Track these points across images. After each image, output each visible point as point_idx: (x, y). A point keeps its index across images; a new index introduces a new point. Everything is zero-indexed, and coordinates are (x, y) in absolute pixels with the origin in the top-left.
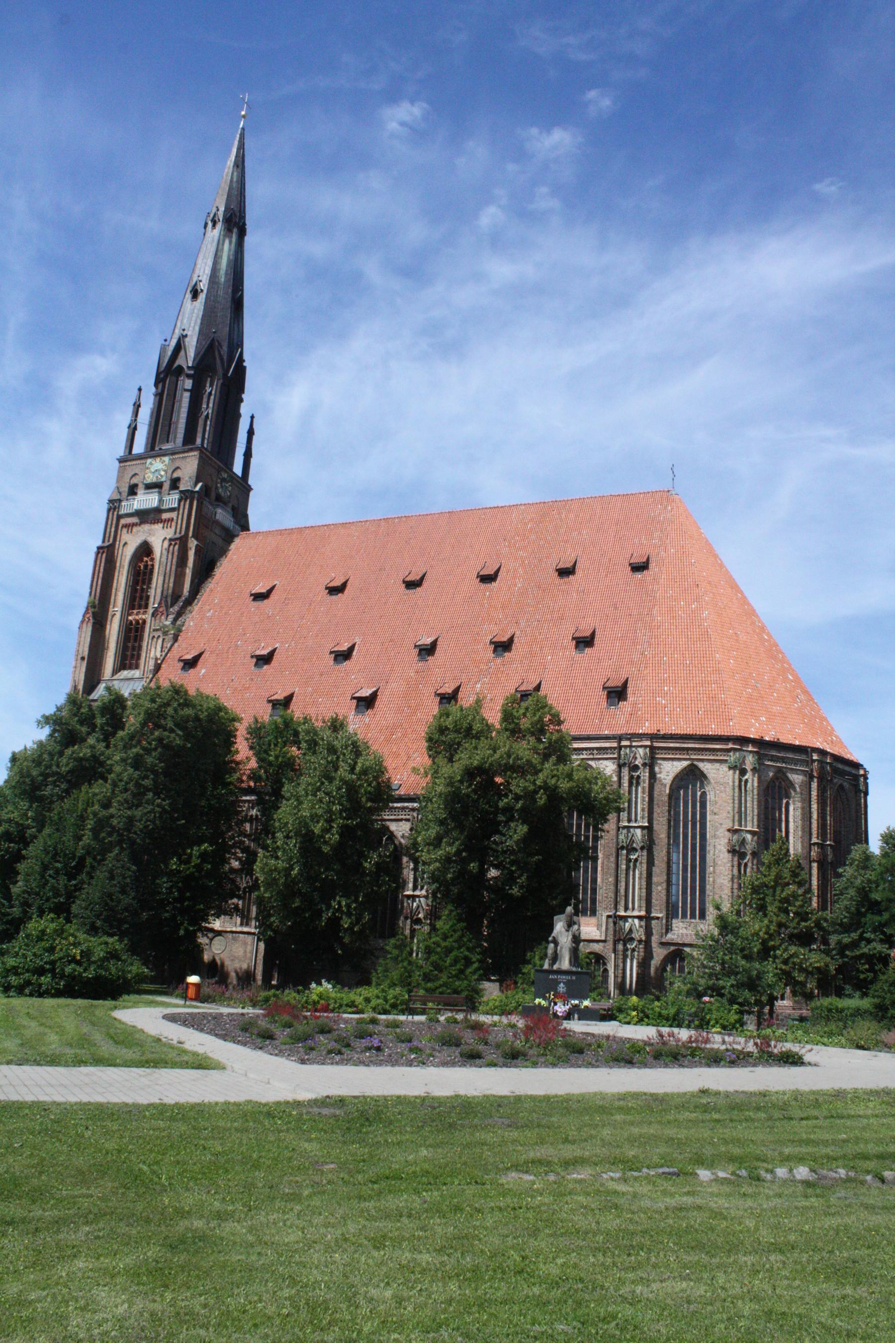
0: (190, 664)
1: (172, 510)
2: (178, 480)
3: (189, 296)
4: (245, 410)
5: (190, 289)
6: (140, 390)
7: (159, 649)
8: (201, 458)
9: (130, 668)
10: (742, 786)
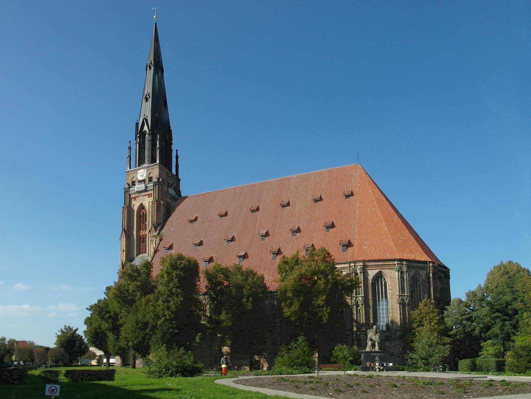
0: (171, 248)
1: (151, 190)
2: (152, 178)
3: (144, 100)
4: (174, 147)
5: (144, 97)
6: (130, 142)
7: (154, 245)
8: (160, 168)
9: (143, 253)
10: (402, 279)
